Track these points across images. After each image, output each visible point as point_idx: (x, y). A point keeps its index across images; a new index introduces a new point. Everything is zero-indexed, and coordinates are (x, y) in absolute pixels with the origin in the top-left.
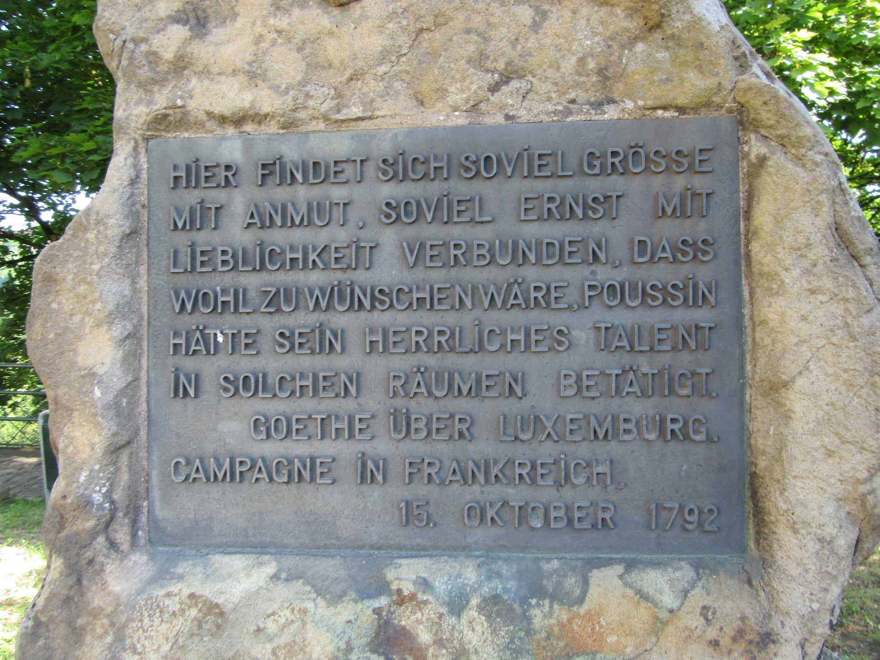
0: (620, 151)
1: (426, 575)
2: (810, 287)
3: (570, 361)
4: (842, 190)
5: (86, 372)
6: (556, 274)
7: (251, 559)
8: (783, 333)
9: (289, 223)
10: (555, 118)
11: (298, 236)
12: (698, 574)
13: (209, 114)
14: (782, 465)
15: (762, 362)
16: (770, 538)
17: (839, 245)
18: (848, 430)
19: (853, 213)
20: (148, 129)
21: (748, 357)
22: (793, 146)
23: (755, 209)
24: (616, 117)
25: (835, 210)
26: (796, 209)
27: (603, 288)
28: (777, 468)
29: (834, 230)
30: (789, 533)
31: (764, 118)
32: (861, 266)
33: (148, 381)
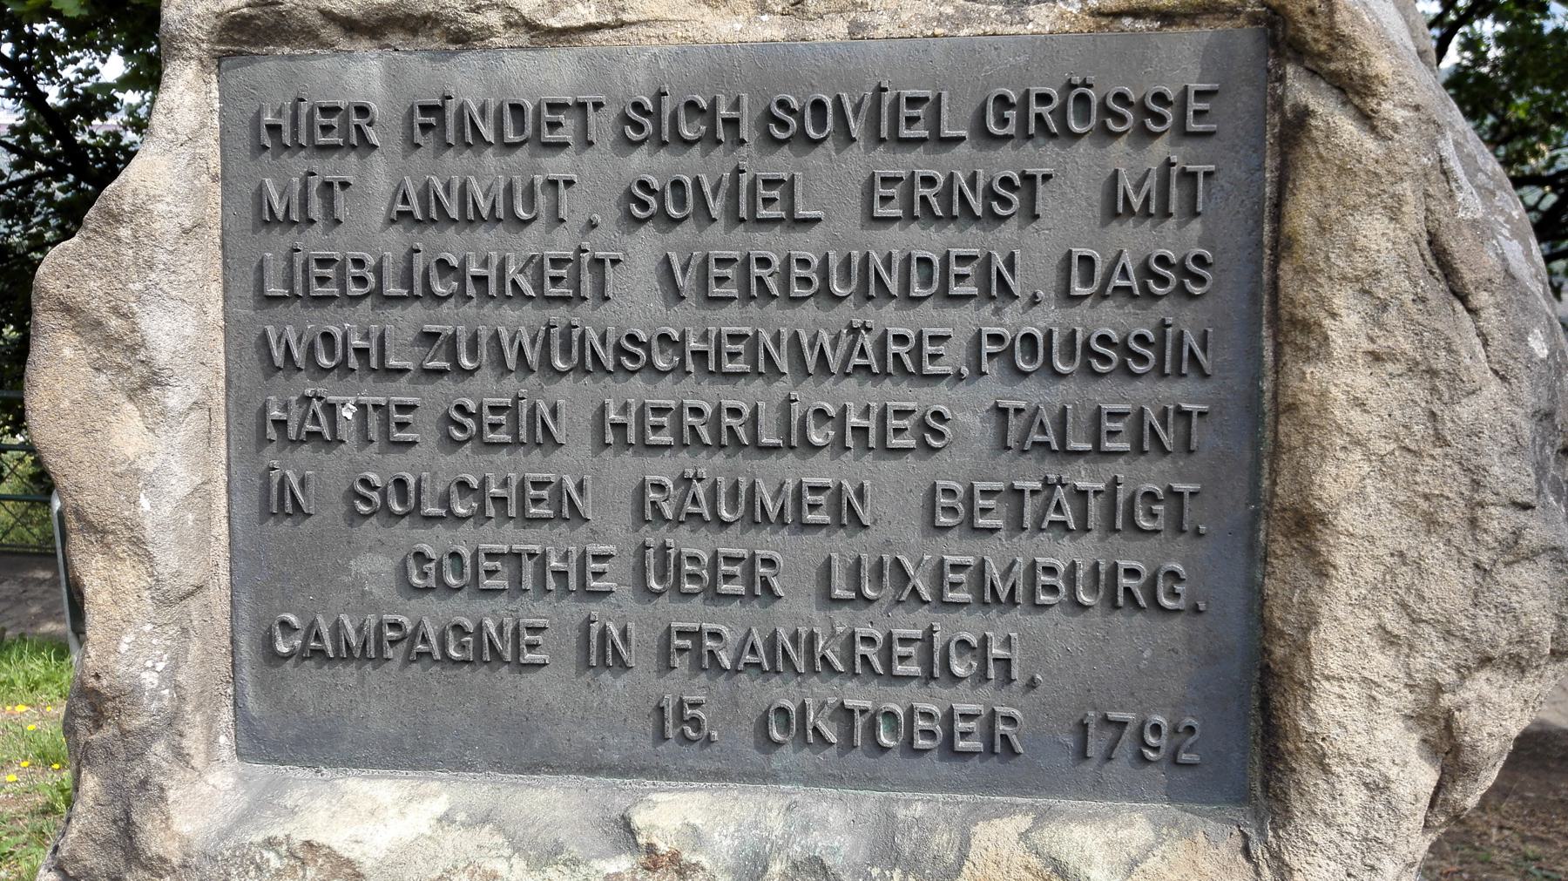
0: (1054, 93)
1: (698, 822)
2: (1371, 347)
3: (950, 470)
4: (1444, 172)
5: (124, 467)
6: (930, 318)
8: (1322, 428)
9: (472, 219)
10: (938, 31)
11: (488, 241)
12: (1158, 835)
13: (329, 16)
14: (1308, 657)
15: (1285, 477)
16: (1285, 779)
17: (1432, 273)
18: (1422, 598)
19: (1461, 215)
20: (221, 41)
21: (1266, 464)
22: (1358, 93)
23: (1289, 204)
25: (1427, 209)
26: (1355, 207)
27: (1013, 340)
28: (1300, 663)
29: (1424, 244)
30: (1315, 772)
31: (1309, 38)
32: (1470, 311)
33: (229, 483)
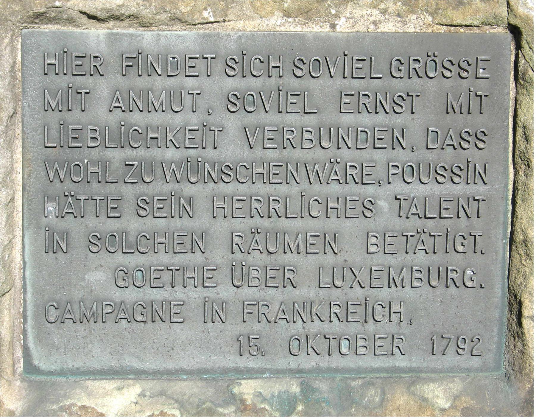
7: (118, 383)
11: (156, 118)
24: (393, 31)
